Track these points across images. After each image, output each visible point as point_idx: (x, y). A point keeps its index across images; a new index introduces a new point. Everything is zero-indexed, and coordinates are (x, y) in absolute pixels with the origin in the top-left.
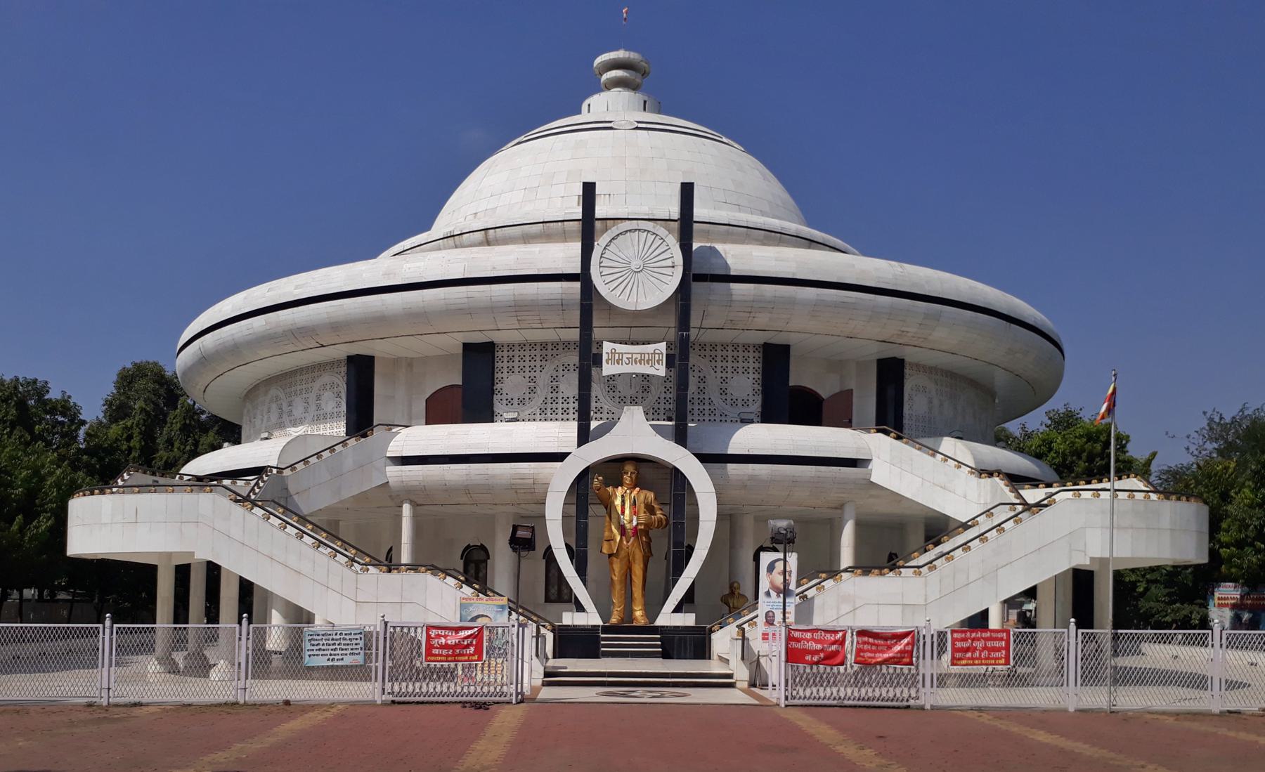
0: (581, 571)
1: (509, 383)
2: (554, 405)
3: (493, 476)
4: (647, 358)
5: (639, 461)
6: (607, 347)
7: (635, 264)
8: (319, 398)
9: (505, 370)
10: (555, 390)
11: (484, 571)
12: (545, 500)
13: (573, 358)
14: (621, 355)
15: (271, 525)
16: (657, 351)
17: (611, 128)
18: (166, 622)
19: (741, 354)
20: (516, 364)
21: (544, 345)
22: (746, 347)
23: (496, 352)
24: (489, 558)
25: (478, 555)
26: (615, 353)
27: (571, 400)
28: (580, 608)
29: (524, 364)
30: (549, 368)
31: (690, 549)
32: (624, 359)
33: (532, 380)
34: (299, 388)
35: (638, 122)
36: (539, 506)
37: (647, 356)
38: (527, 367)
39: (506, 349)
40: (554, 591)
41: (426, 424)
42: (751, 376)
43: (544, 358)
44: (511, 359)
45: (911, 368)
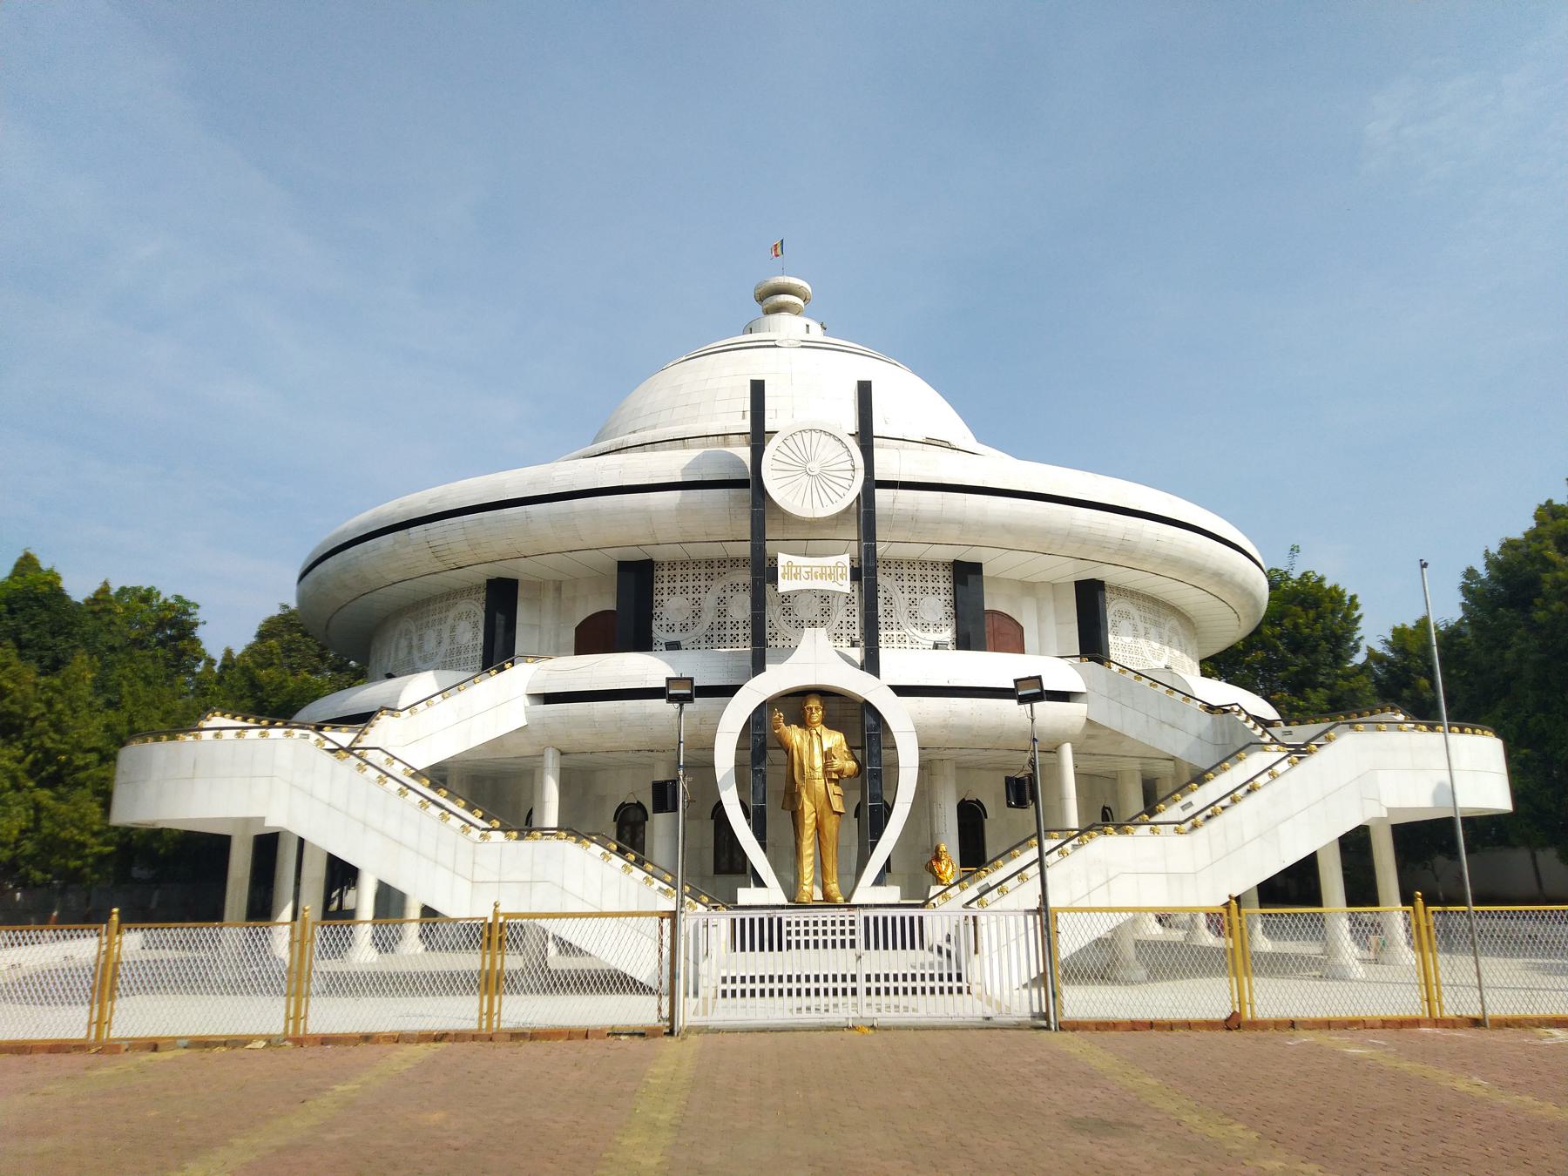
0: (760, 834)
1: (671, 606)
2: (722, 632)
3: (652, 715)
4: (828, 572)
5: (825, 694)
6: (783, 559)
7: (814, 467)
8: (453, 629)
9: (666, 591)
10: (722, 613)
11: (641, 836)
12: (714, 743)
13: (744, 577)
14: (798, 569)
15: (367, 779)
16: (839, 564)
17: (776, 346)
18: (1092, 765)
19: (929, 572)
20: (678, 584)
21: (709, 563)
22: (935, 565)
23: (655, 584)
24: (647, 820)
25: (633, 816)
26: (792, 566)
27: (741, 625)
28: (760, 883)
29: (687, 584)
30: (716, 587)
31: (889, 810)
32: (803, 573)
33: (697, 602)
34: (431, 618)
35: (802, 341)
36: (706, 752)
37: (828, 569)
38: (691, 575)
39: (666, 567)
40: (724, 859)
41: (575, 655)
42: (942, 597)
43: (709, 577)
44: (672, 579)
45: (1112, 592)
